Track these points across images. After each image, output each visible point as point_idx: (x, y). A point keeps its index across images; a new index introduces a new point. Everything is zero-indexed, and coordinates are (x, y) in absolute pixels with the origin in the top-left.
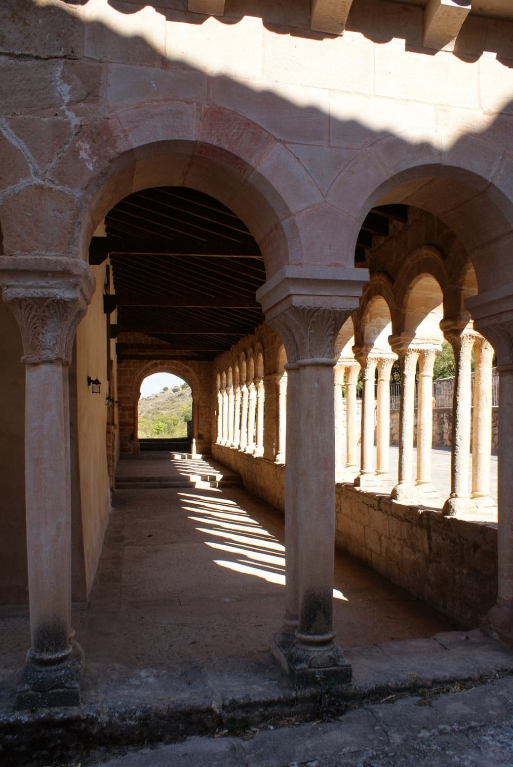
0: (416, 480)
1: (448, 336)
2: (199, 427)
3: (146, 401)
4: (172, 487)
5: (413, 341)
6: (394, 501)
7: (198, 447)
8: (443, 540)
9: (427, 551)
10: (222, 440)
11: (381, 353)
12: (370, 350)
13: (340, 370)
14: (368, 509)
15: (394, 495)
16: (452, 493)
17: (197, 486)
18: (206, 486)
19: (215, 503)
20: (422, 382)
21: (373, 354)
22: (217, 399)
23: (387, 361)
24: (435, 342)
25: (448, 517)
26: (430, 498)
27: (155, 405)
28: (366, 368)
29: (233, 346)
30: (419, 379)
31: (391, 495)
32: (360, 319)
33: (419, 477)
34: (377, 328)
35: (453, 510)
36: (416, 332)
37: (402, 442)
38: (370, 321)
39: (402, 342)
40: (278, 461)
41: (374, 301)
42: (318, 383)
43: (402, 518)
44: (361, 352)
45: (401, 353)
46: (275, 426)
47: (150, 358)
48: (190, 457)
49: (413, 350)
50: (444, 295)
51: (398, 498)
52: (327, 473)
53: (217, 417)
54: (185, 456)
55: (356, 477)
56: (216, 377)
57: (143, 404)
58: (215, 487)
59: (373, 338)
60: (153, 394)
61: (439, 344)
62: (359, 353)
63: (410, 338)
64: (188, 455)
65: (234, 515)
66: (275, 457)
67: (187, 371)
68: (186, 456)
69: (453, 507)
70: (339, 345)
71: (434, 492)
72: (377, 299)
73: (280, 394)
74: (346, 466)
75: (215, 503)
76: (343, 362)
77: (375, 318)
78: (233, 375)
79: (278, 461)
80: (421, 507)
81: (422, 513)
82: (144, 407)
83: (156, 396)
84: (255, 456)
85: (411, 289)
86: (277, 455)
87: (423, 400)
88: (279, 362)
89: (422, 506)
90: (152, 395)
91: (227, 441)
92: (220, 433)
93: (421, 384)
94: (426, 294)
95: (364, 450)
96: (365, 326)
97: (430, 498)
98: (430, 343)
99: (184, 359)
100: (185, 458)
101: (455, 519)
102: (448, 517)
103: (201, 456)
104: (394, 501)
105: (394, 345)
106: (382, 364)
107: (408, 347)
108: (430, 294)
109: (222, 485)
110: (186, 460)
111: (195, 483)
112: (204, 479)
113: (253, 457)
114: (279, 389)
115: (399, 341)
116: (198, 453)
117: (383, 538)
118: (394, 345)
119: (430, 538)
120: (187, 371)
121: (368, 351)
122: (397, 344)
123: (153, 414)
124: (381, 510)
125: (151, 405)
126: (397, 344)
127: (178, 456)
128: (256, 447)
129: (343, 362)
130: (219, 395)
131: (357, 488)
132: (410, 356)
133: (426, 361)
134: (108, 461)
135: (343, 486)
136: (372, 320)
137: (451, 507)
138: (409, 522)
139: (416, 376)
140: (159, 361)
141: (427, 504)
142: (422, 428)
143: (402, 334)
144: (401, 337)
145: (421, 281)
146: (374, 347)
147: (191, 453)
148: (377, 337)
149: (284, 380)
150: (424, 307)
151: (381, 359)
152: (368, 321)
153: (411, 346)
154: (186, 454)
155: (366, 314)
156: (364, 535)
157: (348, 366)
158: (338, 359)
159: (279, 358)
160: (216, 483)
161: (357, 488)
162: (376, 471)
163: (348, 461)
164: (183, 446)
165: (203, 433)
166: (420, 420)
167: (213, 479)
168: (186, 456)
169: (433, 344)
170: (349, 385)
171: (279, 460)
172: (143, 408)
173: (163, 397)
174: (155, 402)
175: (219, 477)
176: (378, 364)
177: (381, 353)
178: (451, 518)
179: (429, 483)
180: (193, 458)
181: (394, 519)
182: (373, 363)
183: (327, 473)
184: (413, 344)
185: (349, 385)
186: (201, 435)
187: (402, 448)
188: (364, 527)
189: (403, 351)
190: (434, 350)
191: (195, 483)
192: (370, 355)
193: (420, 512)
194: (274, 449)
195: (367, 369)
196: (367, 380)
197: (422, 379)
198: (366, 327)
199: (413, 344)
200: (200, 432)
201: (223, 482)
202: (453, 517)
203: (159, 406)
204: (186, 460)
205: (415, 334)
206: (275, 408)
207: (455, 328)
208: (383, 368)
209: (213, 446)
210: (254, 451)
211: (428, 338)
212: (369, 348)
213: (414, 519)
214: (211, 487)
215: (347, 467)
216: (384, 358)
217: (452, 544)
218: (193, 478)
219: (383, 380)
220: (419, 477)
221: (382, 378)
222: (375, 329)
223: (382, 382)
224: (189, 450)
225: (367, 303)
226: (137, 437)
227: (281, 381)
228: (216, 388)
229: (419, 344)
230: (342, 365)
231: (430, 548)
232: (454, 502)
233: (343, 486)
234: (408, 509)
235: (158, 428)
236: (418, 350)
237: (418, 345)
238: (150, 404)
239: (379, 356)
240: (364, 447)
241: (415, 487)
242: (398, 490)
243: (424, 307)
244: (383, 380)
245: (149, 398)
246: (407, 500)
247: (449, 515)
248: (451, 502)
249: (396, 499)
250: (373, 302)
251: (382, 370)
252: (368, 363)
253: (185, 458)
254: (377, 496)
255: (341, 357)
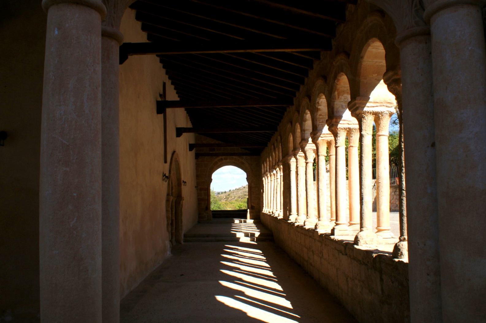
0: (376, 228)
1: (391, 87)
2: (252, 201)
3: (238, 191)
4: (219, 241)
5: (368, 104)
6: (356, 246)
7: (251, 214)
8: (392, 283)
9: (380, 292)
10: (266, 210)
11: (349, 124)
12: (339, 121)
13: (323, 144)
14: (339, 254)
15: (356, 241)
16: (401, 236)
17: (241, 240)
18: (247, 240)
19: (247, 252)
20: (378, 140)
21: (342, 125)
22: (262, 181)
23: (355, 131)
24: (388, 105)
25: (396, 260)
26: (388, 244)
27: (243, 193)
28: (337, 137)
29: (269, 143)
30: (376, 138)
31: (354, 241)
32: (330, 97)
33: (379, 225)
34: (344, 103)
35: (402, 253)
36: (370, 97)
37: (362, 193)
38: (339, 98)
39: (357, 106)
40: (290, 220)
41: (339, 79)
42: (59, 29)
43: (361, 262)
44: (332, 123)
45: (358, 115)
46: (288, 195)
47: (217, 155)
48: (245, 222)
49: (368, 112)
50: (386, 52)
51: (359, 244)
52: (68, 169)
53: (263, 194)
54: (242, 221)
55: (332, 228)
56: (261, 166)
57: (236, 192)
58: (253, 241)
59: (342, 112)
60: (242, 186)
61: (392, 107)
62: (331, 124)
63: (365, 102)
64: (244, 220)
65: (255, 261)
66: (289, 217)
67: (243, 163)
68: (243, 221)
69: (401, 250)
70: (321, 124)
71: (392, 238)
72: (341, 76)
73: (291, 171)
74: (349, 224)
75: (247, 252)
76: (324, 137)
77: (342, 95)
78: (269, 163)
79: (290, 220)
80: (377, 251)
81: (376, 256)
82: (236, 194)
83: (244, 187)
84: (279, 218)
85: (362, 57)
86: (290, 216)
87: (380, 156)
88: (289, 147)
89: (377, 250)
90: (241, 187)
91: (316, 221)
92: (264, 205)
93: (378, 143)
94: (376, 62)
95: (338, 205)
96: (334, 102)
97: (388, 244)
98: (383, 105)
99: (240, 155)
100: (242, 223)
101: (402, 262)
102: (396, 260)
103: (252, 221)
104: (356, 246)
105: (352, 109)
106: (351, 133)
107: (363, 109)
108: (381, 62)
109: (259, 239)
110: (243, 223)
111: (239, 238)
112: (247, 235)
113: (278, 218)
114: (290, 167)
115: (355, 105)
116: (251, 219)
117: (349, 279)
118: (352, 109)
119: (382, 280)
120: (243, 163)
121: (337, 123)
122: (355, 108)
123: (242, 198)
124: (346, 254)
125: (241, 193)
126: (355, 108)
127: (237, 221)
128: (307, 218)
129: (324, 137)
130: (264, 179)
131: (332, 237)
132: (366, 118)
133: (382, 122)
134: (167, 221)
135: (324, 235)
136: (340, 97)
137: (399, 250)
138: (366, 265)
139: (374, 136)
140: (223, 157)
141: (381, 249)
142: (380, 181)
143: (357, 98)
144: (356, 101)
145: (370, 49)
146: (343, 119)
147: (247, 219)
148: (345, 111)
149: (293, 161)
150: (376, 75)
151: (350, 129)
152: (337, 98)
153: (366, 109)
154: (243, 220)
155: (335, 91)
156: (337, 276)
157: (329, 140)
158: (320, 135)
159: (289, 144)
160: (255, 238)
161: (332, 237)
162: (349, 222)
163: (351, 220)
164: (241, 214)
165: (254, 205)
166: (378, 174)
167: (253, 235)
168: (243, 221)
169: (387, 107)
170: (331, 155)
171: (291, 220)
172: (236, 195)
173: (228, 182)
174: (243, 191)
175: (257, 234)
176: (347, 134)
177: (349, 124)
178: (399, 261)
179: (388, 230)
180: (247, 222)
181: (355, 262)
182: (343, 132)
183: (68, 169)
184: (368, 107)
185: (331, 155)
186: (254, 207)
187: (296, 171)
188: (337, 269)
189: (360, 113)
190: (388, 112)
191: (239, 238)
192: (339, 126)
193: (374, 255)
194: (288, 211)
195: (338, 138)
196: (338, 147)
197: (378, 138)
198: (335, 103)
199: (368, 107)
200: (252, 204)
201: (261, 237)
202: (401, 260)
203: (246, 193)
204: (243, 223)
205: (369, 98)
206: (288, 181)
207: (396, 77)
208: (352, 137)
209: (261, 214)
210: (279, 215)
211: (382, 102)
212: (339, 120)
213: (369, 262)
214: (251, 241)
215: (331, 221)
216: (352, 128)
217: (400, 287)
218: (238, 235)
219: (352, 147)
220: (379, 225)
221: (351, 145)
222: (344, 104)
223: (351, 148)
224: (245, 217)
225: (334, 82)
226: (210, 208)
227: (291, 161)
228: (262, 173)
229: (373, 107)
230: (324, 140)
231: (382, 290)
232: (402, 245)
233: (324, 235)
234: (365, 253)
235: (240, 206)
236: (373, 112)
237: (372, 108)
238: (240, 192)
239: (347, 126)
240: (338, 203)
241: (375, 234)
242: (359, 237)
243: (376, 75)
244: (352, 147)
245: (240, 189)
246: (367, 245)
247: (397, 258)
248: (399, 245)
249: (357, 245)
250: (338, 80)
251: (351, 138)
252: (339, 132)
253: (242, 223)
254: (344, 242)
255: (323, 133)
